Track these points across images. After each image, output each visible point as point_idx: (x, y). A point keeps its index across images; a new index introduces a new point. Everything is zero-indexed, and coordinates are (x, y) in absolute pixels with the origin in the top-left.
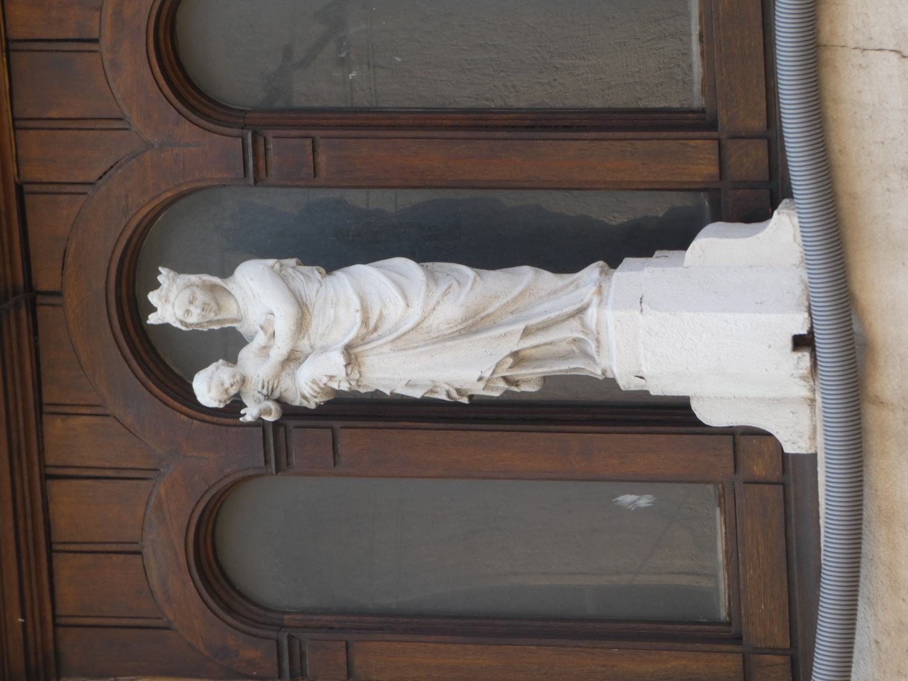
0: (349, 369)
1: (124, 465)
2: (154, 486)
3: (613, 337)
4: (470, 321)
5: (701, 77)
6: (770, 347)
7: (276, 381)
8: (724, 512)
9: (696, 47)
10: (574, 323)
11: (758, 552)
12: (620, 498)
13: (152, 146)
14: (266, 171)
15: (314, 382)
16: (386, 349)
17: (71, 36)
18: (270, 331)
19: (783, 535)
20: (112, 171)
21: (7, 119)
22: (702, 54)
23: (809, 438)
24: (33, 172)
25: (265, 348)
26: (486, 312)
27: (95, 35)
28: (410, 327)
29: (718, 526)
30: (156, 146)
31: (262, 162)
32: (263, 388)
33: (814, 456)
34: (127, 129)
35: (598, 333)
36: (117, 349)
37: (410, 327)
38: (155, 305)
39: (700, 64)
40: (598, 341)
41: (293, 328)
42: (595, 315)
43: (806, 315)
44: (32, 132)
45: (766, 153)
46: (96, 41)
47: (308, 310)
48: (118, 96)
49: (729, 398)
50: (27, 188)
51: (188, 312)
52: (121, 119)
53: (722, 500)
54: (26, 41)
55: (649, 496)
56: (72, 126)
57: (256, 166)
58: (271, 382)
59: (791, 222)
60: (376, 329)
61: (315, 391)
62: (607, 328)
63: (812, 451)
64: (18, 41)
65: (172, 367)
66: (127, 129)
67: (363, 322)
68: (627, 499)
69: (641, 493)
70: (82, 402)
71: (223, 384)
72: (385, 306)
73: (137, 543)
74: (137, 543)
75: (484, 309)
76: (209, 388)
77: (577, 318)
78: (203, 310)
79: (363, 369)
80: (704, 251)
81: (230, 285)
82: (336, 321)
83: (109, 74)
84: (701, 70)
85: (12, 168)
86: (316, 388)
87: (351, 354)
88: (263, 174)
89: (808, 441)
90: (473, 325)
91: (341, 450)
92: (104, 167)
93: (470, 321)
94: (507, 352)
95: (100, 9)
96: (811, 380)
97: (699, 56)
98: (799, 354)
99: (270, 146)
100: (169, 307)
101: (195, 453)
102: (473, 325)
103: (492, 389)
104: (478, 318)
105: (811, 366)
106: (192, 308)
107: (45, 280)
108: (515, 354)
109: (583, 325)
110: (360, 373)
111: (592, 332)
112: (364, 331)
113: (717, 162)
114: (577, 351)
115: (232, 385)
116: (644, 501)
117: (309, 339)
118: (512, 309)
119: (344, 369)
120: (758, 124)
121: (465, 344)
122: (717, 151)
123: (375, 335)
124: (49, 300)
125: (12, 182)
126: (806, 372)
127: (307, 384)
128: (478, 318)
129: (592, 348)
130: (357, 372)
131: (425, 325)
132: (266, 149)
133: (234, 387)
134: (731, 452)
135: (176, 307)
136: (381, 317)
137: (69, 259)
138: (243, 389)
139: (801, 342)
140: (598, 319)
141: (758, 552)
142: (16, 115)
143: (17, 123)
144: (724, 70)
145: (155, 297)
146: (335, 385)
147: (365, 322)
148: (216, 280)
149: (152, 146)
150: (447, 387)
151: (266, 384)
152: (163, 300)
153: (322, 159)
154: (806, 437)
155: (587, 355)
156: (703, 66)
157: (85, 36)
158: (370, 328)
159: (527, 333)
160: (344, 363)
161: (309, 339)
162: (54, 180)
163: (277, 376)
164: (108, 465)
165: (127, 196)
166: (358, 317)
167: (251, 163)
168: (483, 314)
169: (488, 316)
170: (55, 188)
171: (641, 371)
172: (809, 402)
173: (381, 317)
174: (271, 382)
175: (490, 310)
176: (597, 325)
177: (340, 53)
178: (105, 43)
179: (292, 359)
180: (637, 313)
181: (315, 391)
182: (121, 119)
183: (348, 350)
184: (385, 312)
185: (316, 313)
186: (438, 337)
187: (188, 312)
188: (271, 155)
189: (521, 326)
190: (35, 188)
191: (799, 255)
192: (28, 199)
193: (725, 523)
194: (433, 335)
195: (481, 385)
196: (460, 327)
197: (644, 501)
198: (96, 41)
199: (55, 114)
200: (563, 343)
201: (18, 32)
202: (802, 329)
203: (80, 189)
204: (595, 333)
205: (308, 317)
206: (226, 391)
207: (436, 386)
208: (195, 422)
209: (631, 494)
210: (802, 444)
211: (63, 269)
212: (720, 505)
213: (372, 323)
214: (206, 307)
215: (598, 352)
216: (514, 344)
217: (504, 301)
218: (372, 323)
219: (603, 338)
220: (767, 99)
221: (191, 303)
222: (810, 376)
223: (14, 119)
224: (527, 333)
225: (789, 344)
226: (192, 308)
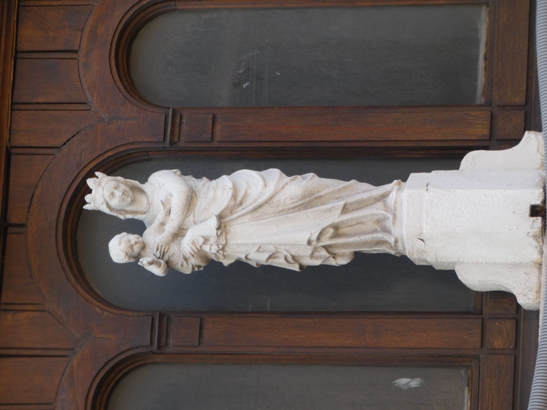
0: (219, 232)
1: (51, 346)
2: (70, 361)
3: (404, 212)
4: (307, 199)
5: (483, 83)
6: (514, 213)
7: (167, 247)
8: (470, 391)
9: (481, 64)
10: (380, 204)
11: (492, 405)
12: (398, 381)
13: (104, 120)
14: (179, 137)
15: (193, 243)
16: (247, 218)
17: (60, 48)
18: (168, 207)
19: (511, 392)
20: (74, 139)
21: (8, 102)
22: (485, 68)
23: (536, 292)
24: (20, 140)
25: (163, 224)
26: (319, 194)
27: (76, 48)
28: (266, 217)
29: (466, 401)
30: (106, 120)
31: (177, 130)
32: (157, 250)
33: (537, 312)
34: (89, 110)
35: (395, 210)
36: (63, 105)
37: (266, 217)
38: (91, 188)
39: (483, 75)
40: (394, 215)
41: (184, 202)
42: (394, 197)
43: (542, 190)
44: (23, 112)
45: (523, 119)
46: (76, 52)
47: (196, 195)
48: (85, 87)
49: (482, 264)
50: (13, 151)
51: (112, 194)
52: (85, 103)
53: (470, 382)
54: (29, 52)
55: (418, 379)
56: (51, 108)
57: (172, 131)
58: (163, 247)
59: (537, 138)
60: (241, 204)
61: (193, 250)
62: (402, 205)
63: (537, 309)
64: (24, 52)
65: (94, 289)
66: (89, 110)
67: (233, 196)
68: (402, 382)
69: (413, 377)
70: (28, 302)
71: (130, 241)
72: (249, 187)
73: (51, 404)
74: (51, 404)
75: (318, 192)
76: (118, 248)
77: (381, 201)
78: (123, 193)
79: (229, 237)
80: (474, 160)
81: (145, 187)
82: (214, 198)
83: (82, 73)
84: (484, 79)
85: (6, 135)
86: (195, 250)
87: (222, 225)
88: (176, 139)
89: (535, 294)
90: (308, 202)
91: (205, 333)
92: (68, 136)
93: (307, 199)
94: (330, 222)
95: (82, 30)
96: (540, 240)
97: (485, 44)
98: (534, 218)
99: (184, 121)
100: (100, 189)
101: (102, 336)
102: (308, 202)
103: (317, 258)
104: (313, 197)
105: (542, 227)
106: (116, 192)
107: (14, 217)
108: (336, 227)
109: (385, 206)
110: (226, 239)
111: (391, 210)
112: (232, 203)
113: (489, 127)
114: (379, 229)
115: (136, 243)
116: (415, 383)
117: (194, 216)
118: (337, 196)
119: (216, 230)
120: (520, 100)
121: (302, 215)
122: (489, 118)
123: (240, 208)
124: (17, 230)
125: (5, 144)
126: (538, 230)
127: (188, 245)
128: (313, 197)
129: (389, 224)
130: (224, 238)
131: (276, 199)
132: (181, 122)
133: (137, 245)
134: (479, 331)
135: (105, 190)
136: (246, 195)
137: (35, 199)
138: (143, 253)
139: (535, 211)
140: (396, 199)
141: (492, 405)
142: (14, 100)
143: (14, 106)
144: (500, 63)
145: (90, 181)
146: (206, 248)
147: (234, 197)
148: (137, 183)
149: (104, 120)
150: (285, 253)
151: (160, 247)
152: (97, 184)
153: (218, 128)
154: (535, 291)
155: (387, 231)
156: (485, 77)
157: (69, 48)
158: (237, 201)
159: (345, 210)
160: (217, 227)
161: (194, 216)
162: (33, 145)
163: (168, 244)
164: (39, 346)
165: (81, 154)
166: (230, 193)
167: (169, 128)
168: (316, 195)
169: (320, 197)
170: (33, 150)
171: (421, 233)
172: (538, 266)
173: (246, 195)
174: (163, 247)
175: (322, 193)
176: (395, 203)
177: (240, 70)
178: (82, 53)
179: (179, 233)
180: (424, 191)
181: (193, 250)
182: (85, 103)
183: (220, 217)
184: (249, 191)
185: (201, 196)
186: (283, 211)
187: (112, 194)
188: (185, 128)
189: (342, 203)
190: (20, 151)
191: (540, 161)
192: (13, 158)
193: (471, 399)
194: (280, 208)
195: (309, 250)
196: (300, 203)
197: (415, 383)
198: (76, 52)
199: (41, 100)
200: (370, 222)
201: (24, 46)
202: (538, 200)
203: (50, 151)
204: (393, 210)
205: (195, 200)
206: (132, 246)
207: (278, 252)
208: (105, 313)
209: (406, 378)
210: (531, 296)
211: (29, 208)
212: (468, 386)
213: (239, 199)
214: (125, 193)
215: (394, 223)
216: (335, 218)
217: (333, 189)
218: (239, 199)
219: (398, 214)
220: (527, 85)
221: (116, 188)
222: (540, 236)
223: (12, 103)
224: (345, 210)
225: (528, 211)
226: (116, 192)
